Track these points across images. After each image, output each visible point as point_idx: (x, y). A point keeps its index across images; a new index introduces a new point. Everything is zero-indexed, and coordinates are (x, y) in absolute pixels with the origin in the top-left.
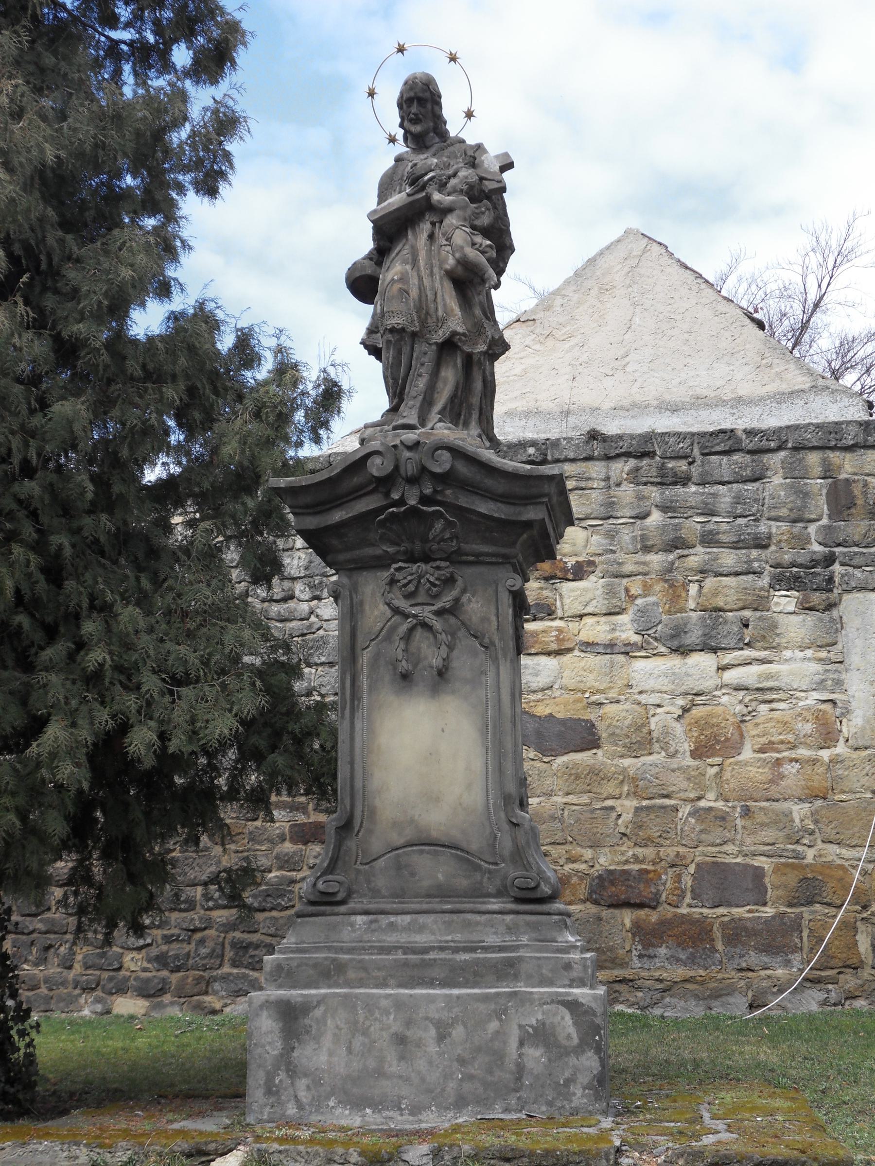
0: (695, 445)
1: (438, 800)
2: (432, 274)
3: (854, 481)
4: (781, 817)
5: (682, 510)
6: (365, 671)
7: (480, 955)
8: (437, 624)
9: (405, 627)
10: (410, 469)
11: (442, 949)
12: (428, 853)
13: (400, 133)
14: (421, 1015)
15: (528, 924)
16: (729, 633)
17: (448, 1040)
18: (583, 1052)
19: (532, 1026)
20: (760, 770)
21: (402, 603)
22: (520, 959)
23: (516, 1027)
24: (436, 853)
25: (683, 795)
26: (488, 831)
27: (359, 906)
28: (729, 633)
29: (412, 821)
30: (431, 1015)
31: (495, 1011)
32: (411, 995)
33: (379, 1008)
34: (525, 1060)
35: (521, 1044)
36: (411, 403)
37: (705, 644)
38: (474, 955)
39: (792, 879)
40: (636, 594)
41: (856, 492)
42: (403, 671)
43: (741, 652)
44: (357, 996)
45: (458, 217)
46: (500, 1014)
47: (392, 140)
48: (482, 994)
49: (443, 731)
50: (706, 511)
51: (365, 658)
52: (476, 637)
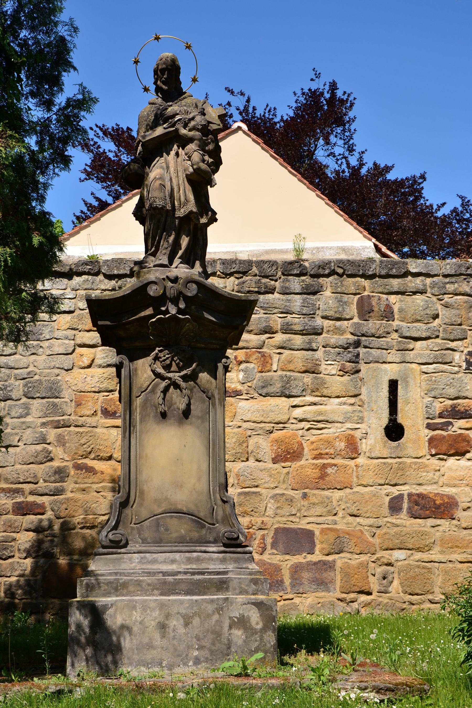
0: (279, 269)
1: (181, 487)
2: (178, 176)
3: (373, 296)
4: (325, 499)
5: (271, 309)
6: (138, 410)
7: (206, 577)
8: (183, 384)
9: (164, 384)
10: (171, 293)
11: (186, 573)
12: (176, 517)
13: (153, 88)
14: (175, 611)
15: (231, 558)
16: (297, 386)
17: (190, 626)
18: (266, 632)
19: (236, 618)
20: (314, 471)
21: (161, 370)
22: (231, 579)
23: (228, 618)
24: (180, 518)
25: (266, 485)
26: (209, 506)
27: (134, 549)
28: (297, 386)
29: (166, 499)
30: (181, 612)
31: (216, 609)
32: (169, 600)
33: (149, 608)
34: (233, 637)
35: (230, 628)
36: (164, 251)
37: (282, 392)
38: (203, 577)
39: (331, 537)
40: (241, 360)
41: (374, 303)
42: (163, 411)
43: (304, 398)
44: (136, 601)
45: (196, 144)
46: (219, 610)
47: (146, 90)
48: (209, 599)
49: (185, 446)
50: (284, 311)
51: (138, 402)
52: (204, 392)
